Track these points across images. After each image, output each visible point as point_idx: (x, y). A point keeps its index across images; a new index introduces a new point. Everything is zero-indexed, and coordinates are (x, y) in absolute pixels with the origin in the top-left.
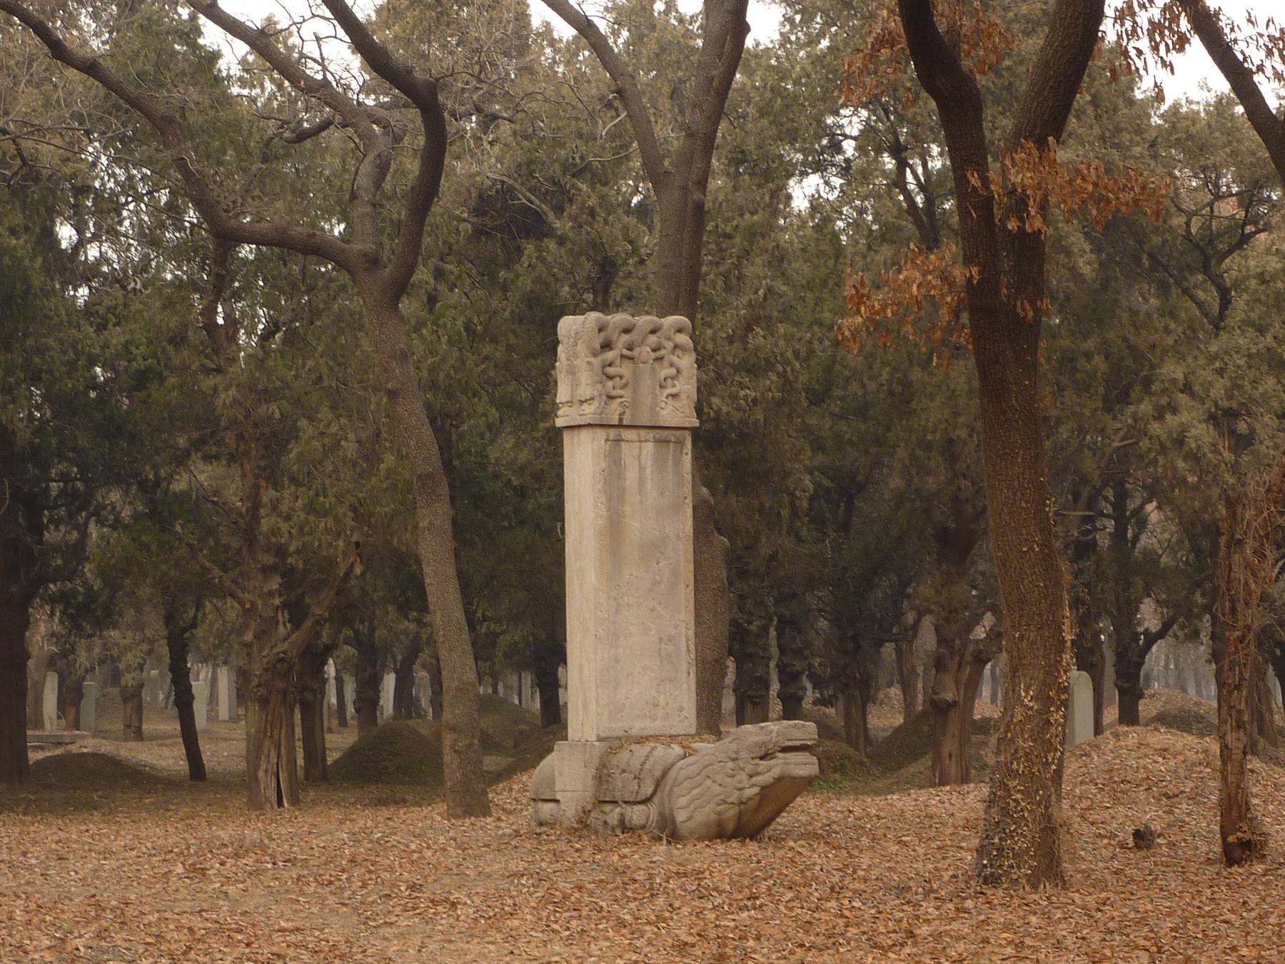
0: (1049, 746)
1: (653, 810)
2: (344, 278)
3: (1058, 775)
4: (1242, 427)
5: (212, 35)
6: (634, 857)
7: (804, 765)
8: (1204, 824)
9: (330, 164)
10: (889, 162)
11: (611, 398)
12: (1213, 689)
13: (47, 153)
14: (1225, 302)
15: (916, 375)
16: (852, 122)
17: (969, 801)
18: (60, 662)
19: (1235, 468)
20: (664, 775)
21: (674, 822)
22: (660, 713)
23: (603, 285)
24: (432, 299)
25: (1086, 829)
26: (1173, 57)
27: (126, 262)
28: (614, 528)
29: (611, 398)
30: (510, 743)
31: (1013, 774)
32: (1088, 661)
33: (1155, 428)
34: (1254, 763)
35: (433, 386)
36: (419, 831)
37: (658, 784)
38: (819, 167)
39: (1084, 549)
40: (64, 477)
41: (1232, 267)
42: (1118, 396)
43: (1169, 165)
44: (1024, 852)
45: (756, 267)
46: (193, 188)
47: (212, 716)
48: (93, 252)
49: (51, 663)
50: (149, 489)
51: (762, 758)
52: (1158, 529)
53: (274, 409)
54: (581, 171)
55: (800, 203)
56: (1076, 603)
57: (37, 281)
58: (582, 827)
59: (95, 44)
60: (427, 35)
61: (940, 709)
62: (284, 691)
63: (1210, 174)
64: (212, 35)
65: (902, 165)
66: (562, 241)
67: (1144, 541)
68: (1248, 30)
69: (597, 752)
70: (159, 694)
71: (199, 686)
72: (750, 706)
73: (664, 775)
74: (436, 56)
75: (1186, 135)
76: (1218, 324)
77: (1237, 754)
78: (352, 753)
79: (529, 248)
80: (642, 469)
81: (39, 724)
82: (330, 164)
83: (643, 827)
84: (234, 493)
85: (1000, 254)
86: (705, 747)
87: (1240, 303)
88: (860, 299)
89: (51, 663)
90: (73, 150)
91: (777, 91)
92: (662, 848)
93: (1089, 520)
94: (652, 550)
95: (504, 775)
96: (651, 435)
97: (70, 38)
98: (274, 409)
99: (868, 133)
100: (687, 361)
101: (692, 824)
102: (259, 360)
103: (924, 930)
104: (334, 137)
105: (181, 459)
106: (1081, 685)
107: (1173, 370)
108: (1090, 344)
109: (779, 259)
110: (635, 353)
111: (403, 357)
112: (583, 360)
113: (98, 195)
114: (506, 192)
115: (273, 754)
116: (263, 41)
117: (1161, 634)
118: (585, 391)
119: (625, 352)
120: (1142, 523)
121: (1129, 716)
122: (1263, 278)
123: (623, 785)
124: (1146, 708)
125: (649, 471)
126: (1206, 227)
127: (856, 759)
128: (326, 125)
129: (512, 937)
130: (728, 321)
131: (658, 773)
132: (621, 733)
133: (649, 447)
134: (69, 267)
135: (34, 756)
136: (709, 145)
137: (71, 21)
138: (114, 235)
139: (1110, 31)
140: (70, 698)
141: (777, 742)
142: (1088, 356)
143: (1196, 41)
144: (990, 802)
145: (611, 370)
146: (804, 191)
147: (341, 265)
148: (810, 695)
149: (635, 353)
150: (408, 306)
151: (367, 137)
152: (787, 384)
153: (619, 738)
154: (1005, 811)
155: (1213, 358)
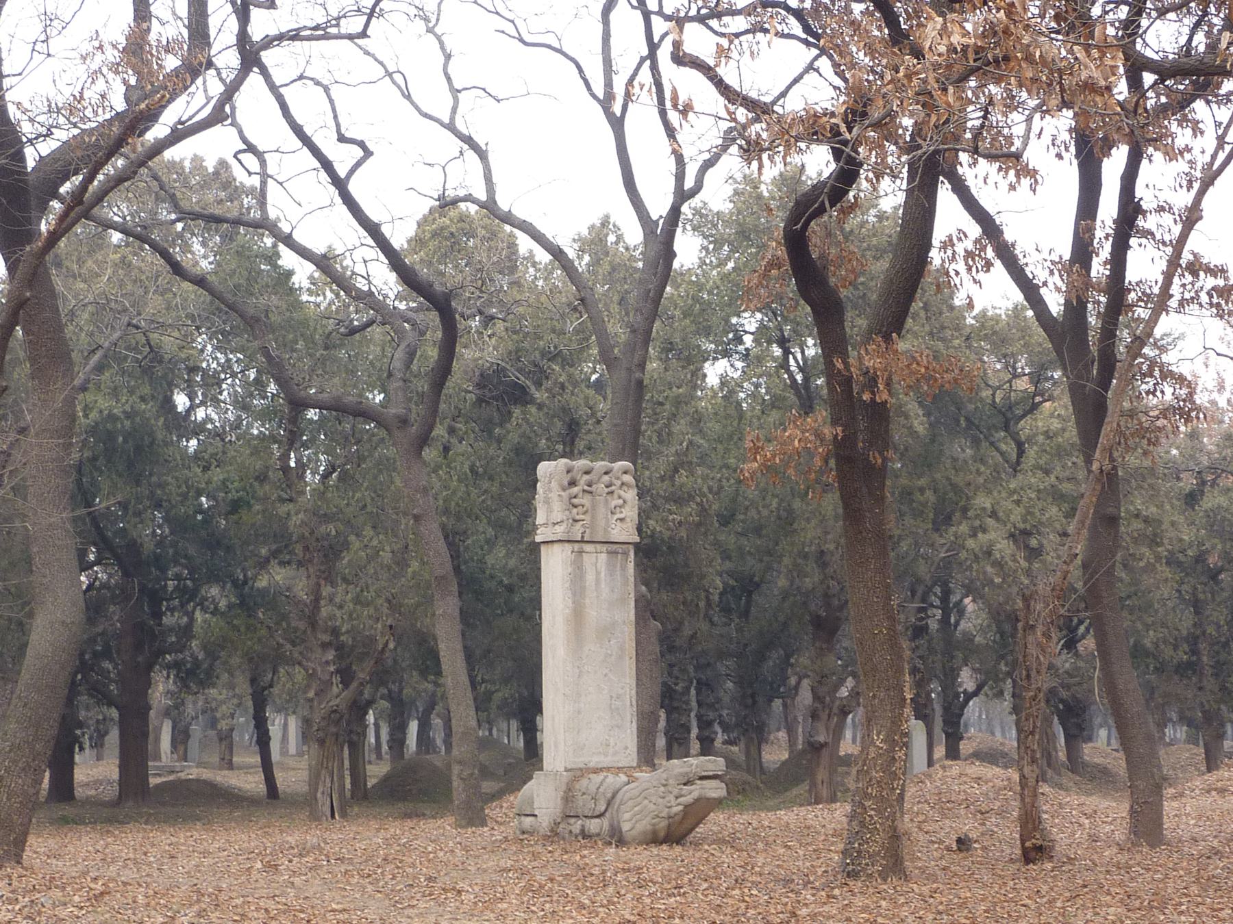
0: (894, 776)
1: (606, 822)
2: (383, 433)
4: (1033, 542)
5: (288, 259)
7: (715, 790)
8: (1008, 833)
9: (373, 351)
10: (777, 351)
11: (576, 521)
13: (168, 342)
14: (1021, 452)
15: (797, 504)
16: (750, 322)
19: (1028, 573)
20: (613, 797)
21: (621, 832)
22: (611, 751)
23: (570, 439)
24: (446, 449)
25: (921, 836)
26: (981, 276)
28: (577, 615)
29: (576, 521)
30: (501, 772)
31: (867, 796)
33: (970, 543)
35: (446, 511)
36: (434, 837)
37: (608, 805)
38: (726, 354)
39: (919, 631)
40: (178, 577)
41: (1025, 427)
42: (943, 520)
43: (979, 353)
44: (878, 853)
45: (681, 426)
46: (274, 368)
47: (284, 752)
48: (200, 414)
49: (167, 713)
51: (685, 784)
52: (973, 617)
53: (331, 529)
56: (914, 671)
57: (160, 435)
58: (553, 835)
60: (444, 258)
61: (815, 748)
62: (338, 734)
63: (1009, 360)
64: (288, 259)
65: (787, 352)
66: (540, 407)
67: (963, 625)
69: (565, 780)
70: (245, 735)
71: (275, 730)
72: (677, 745)
73: (613, 797)
74: (450, 274)
75: (993, 333)
76: (1016, 467)
77: (1032, 782)
78: (386, 779)
79: (517, 412)
80: (598, 573)
81: (157, 757)
82: (373, 351)
83: (598, 835)
84: (301, 589)
85: (859, 422)
86: (644, 776)
88: (757, 450)
89: (167, 713)
90: (187, 340)
91: (697, 299)
92: (612, 850)
93: (921, 610)
94: (606, 631)
96: (604, 548)
98: (331, 529)
99: (762, 328)
100: (631, 495)
101: (634, 832)
102: (320, 493)
103: (804, 912)
104: (376, 331)
105: (263, 564)
106: (917, 730)
107: (983, 501)
108: (922, 482)
109: (698, 420)
110: (593, 489)
114: (500, 371)
115: (328, 780)
116: (324, 263)
117: (976, 693)
119: (586, 488)
120: (961, 612)
121: (953, 753)
122: (1048, 435)
123: (583, 804)
124: (965, 747)
125: (603, 575)
127: (752, 785)
128: (370, 323)
130: (661, 465)
131: (609, 795)
132: (582, 766)
133: (604, 556)
134: (182, 425)
135: (153, 781)
137: (186, 248)
138: (216, 402)
140: (181, 738)
141: (697, 772)
142: (922, 490)
143: (998, 264)
144: (852, 817)
145: (575, 501)
146: (715, 372)
149: (593, 489)
150: (429, 454)
151: (400, 332)
152: (703, 510)
153: (581, 769)
154: (862, 824)
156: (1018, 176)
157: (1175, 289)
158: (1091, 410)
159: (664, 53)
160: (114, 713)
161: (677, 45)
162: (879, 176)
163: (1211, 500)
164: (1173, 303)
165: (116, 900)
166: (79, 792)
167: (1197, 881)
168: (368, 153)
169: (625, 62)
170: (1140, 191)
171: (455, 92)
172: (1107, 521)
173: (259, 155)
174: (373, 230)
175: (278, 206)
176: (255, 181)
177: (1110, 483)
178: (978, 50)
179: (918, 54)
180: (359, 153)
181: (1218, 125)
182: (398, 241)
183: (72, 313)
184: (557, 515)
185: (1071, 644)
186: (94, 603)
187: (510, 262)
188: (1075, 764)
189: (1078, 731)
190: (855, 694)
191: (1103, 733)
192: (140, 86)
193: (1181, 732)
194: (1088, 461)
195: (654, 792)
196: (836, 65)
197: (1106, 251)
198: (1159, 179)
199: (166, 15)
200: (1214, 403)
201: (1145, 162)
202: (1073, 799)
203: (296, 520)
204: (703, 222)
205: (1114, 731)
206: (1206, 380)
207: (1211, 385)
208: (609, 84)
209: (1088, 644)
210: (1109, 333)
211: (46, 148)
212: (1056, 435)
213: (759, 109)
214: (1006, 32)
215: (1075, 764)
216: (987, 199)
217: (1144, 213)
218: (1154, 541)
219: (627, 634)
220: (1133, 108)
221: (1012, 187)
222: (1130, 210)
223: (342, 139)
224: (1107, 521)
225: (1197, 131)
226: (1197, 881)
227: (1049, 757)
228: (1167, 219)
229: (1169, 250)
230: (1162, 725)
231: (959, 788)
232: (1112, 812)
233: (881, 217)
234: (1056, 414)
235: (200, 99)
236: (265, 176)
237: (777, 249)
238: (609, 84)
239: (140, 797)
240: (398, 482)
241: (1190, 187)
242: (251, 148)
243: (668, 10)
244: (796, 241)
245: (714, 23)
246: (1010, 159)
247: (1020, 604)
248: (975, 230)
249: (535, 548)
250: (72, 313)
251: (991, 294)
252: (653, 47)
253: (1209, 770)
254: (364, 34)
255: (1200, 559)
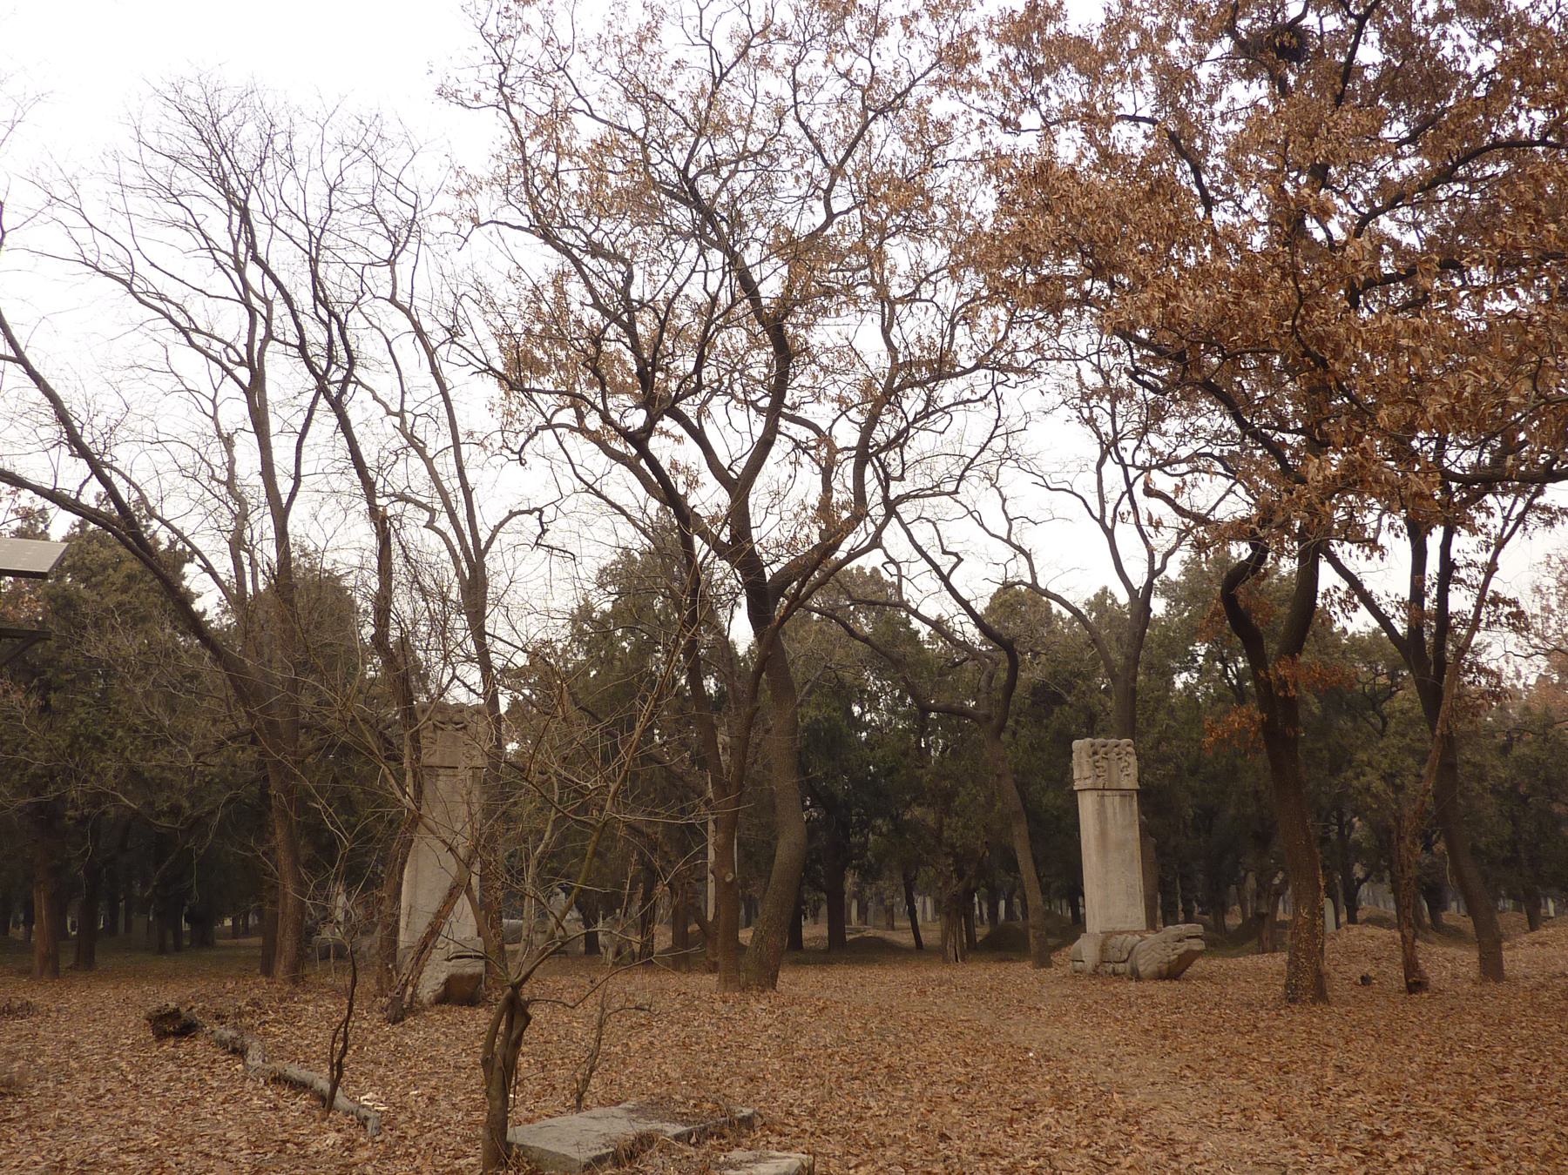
0: (1316, 936)
1: (1128, 965)
2: (975, 725)
3: (1322, 950)
4: (1398, 781)
5: (916, 624)
6: (1119, 987)
7: (1198, 945)
8: (1396, 973)
9: (968, 676)
10: (1219, 665)
12: (1392, 905)
13: (848, 676)
14: (1385, 724)
15: (1239, 762)
16: (1201, 649)
17: (1280, 960)
18: (859, 895)
19: (1396, 801)
23: (1091, 726)
24: (1014, 734)
25: (1337, 976)
26: (1352, 614)
27: (882, 721)
28: (1103, 835)
31: (1300, 950)
32: (1331, 895)
33: (1355, 783)
34: (1418, 943)
35: (1016, 772)
36: (1021, 973)
38: (1187, 669)
39: (1324, 840)
40: (858, 814)
41: (1386, 707)
42: (1335, 770)
43: (1352, 661)
44: (1307, 986)
45: (1161, 715)
46: (910, 689)
47: (924, 919)
48: (868, 717)
49: (855, 896)
50: (894, 819)
52: (1359, 829)
53: (948, 784)
54: (1078, 675)
55: (1179, 685)
56: (1324, 868)
57: (845, 730)
58: (1095, 973)
59: (867, 629)
60: (1007, 619)
61: (1260, 917)
62: (956, 910)
63: (1372, 665)
64: (916, 624)
65: (1226, 667)
66: (1071, 706)
67: (1353, 836)
68: (1387, 599)
70: (901, 908)
71: (918, 906)
72: (1169, 917)
74: (1013, 627)
75: (1360, 647)
76: (1382, 734)
77: (1410, 939)
78: (988, 937)
79: (1057, 710)
81: (850, 923)
82: (968, 676)
84: (931, 819)
85: (1278, 707)
86: (1151, 936)
87: (1392, 724)
88: (1212, 730)
89: (855, 896)
90: (859, 675)
91: (1166, 636)
92: (1133, 984)
93: (1325, 827)
95: (1057, 948)
97: (856, 627)
98: (948, 784)
99: (1208, 651)
100: (1133, 759)
102: (940, 762)
103: (1262, 1025)
104: (969, 664)
105: (908, 806)
106: (1328, 905)
107: (1362, 756)
108: (1320, 745)
109: (1171, 711)
111: (1003, 759)
112: (1085, 759)
113: (869, 693)
114: (1045, 685)
116: (938, 625)
117: (1365, 880)
118: (1087, 773)
120: (1352, 827)
121: (1352, 919)
122: (1401, 712)
123: (1113, 954)
124: (1361, 915)
126: (1373, 689)
127: (1221, 941)
128: (966, 659)
129: (1066, 1025)
130: (1149, 740)
133: (1117, 799)
134: (858, 724)
135: (849, 937)
136: (1137, 662)
137: (856, 620)
138: (877, 710)
139: (1319, 602)
140: (863, 911)
141: (1184, 934)
142: (1321, 750)
143: (1362, 606)
144: (1289, 963)
146: (1180, 680)
147: (974, 720)
148: (1197, 910)
150: (1005, 737)
151: (984, 664)
152: (1178, 767)
154: (1297, 967)
155: (1381, 750)
156: (1371, 551)
157: (1483, 616)
158: (1432, 695)
159: (1138, 489)
160: (824, 896)
161: (1146, 484)
162: (1280, 555)
163: (1518, 750)
164: (1483, 625)
165: (831, 1012)
166: (805, 944)
167: (1532, 1006)
168: (960, 560)
169: (1112, 496)
170: (1453, 554)
171: (1010, 521)
172: (1448, 767)
173: (897, 565)
174: (965, 604)
175: (908, 592)
176: (895, 579)
177: (1449, 743)
178: (1343, 477)
179: (1303, 481)
180: (955, 560)
181: (1503, 509)
182: (980, 607)
183: (793, 662)
184: (1087, 773)
185: (1428, 847)
186: (812, 829)
187: (1049, 618)
188: (1437, 926)
189: (1437, 905)
190: (1285, 882)
191: (1454, 905)
192: (827, 530)
193: (1509, 904)
194: (1433, 729)
195: (1157, 947)
196: (1247, 491)
197: (1434, 593)
198: (1465, 546)
199: (840, 487)
200: (1513, 686)
201: (1455, 536)
202: (1439, 950)
203: (926, 779)
204: (1169, 589)
205: (1462, 903)
206: (1509, 671)
207: (1511, 675)
208: (1103, 510)
209: (1441, 846)
210: (1440, 646)
211: (776, 568)
212: (1408, 711)
213: (1201, 520)
214: (1361, 465)
215: (1437, 926)
216: (1350, 565)
217: (1457, 568)
218: (1481, 779)
219: (1135, 847)
220: (1447, 504)
221: (1368, 558)
222: (1448, 566)
223: (945, 552)
224: (1448, 767)
225: (1490, 514)
226: (1532, 1006)
227: (1419, 923)
228: (1474, 571)
229: (1477, 591)
230: (1496, 899)
231: (1361, 943)
232: (1467, 959)
233: (1282, 579)
234: (1407, 698)
235: (863, 535)
236: (900, 576)
237: (1216, 604)
238: (1103, 510)
239: (843, 949)
240: (987, 755)
241: (1488, 550)
242: (892, 561)
243: (1138, 463)
244: (1229, 598)
245: (1167, 469)
246: (1373, 545)
247: (1391, 822)
248: (1344, 586)
249: (1074, 794)
250: (793, 662)
251: (1361, 623)
252: (1130, 486)
253: (1532, 930)
254: (956, 492)
255: (1514, 788)
